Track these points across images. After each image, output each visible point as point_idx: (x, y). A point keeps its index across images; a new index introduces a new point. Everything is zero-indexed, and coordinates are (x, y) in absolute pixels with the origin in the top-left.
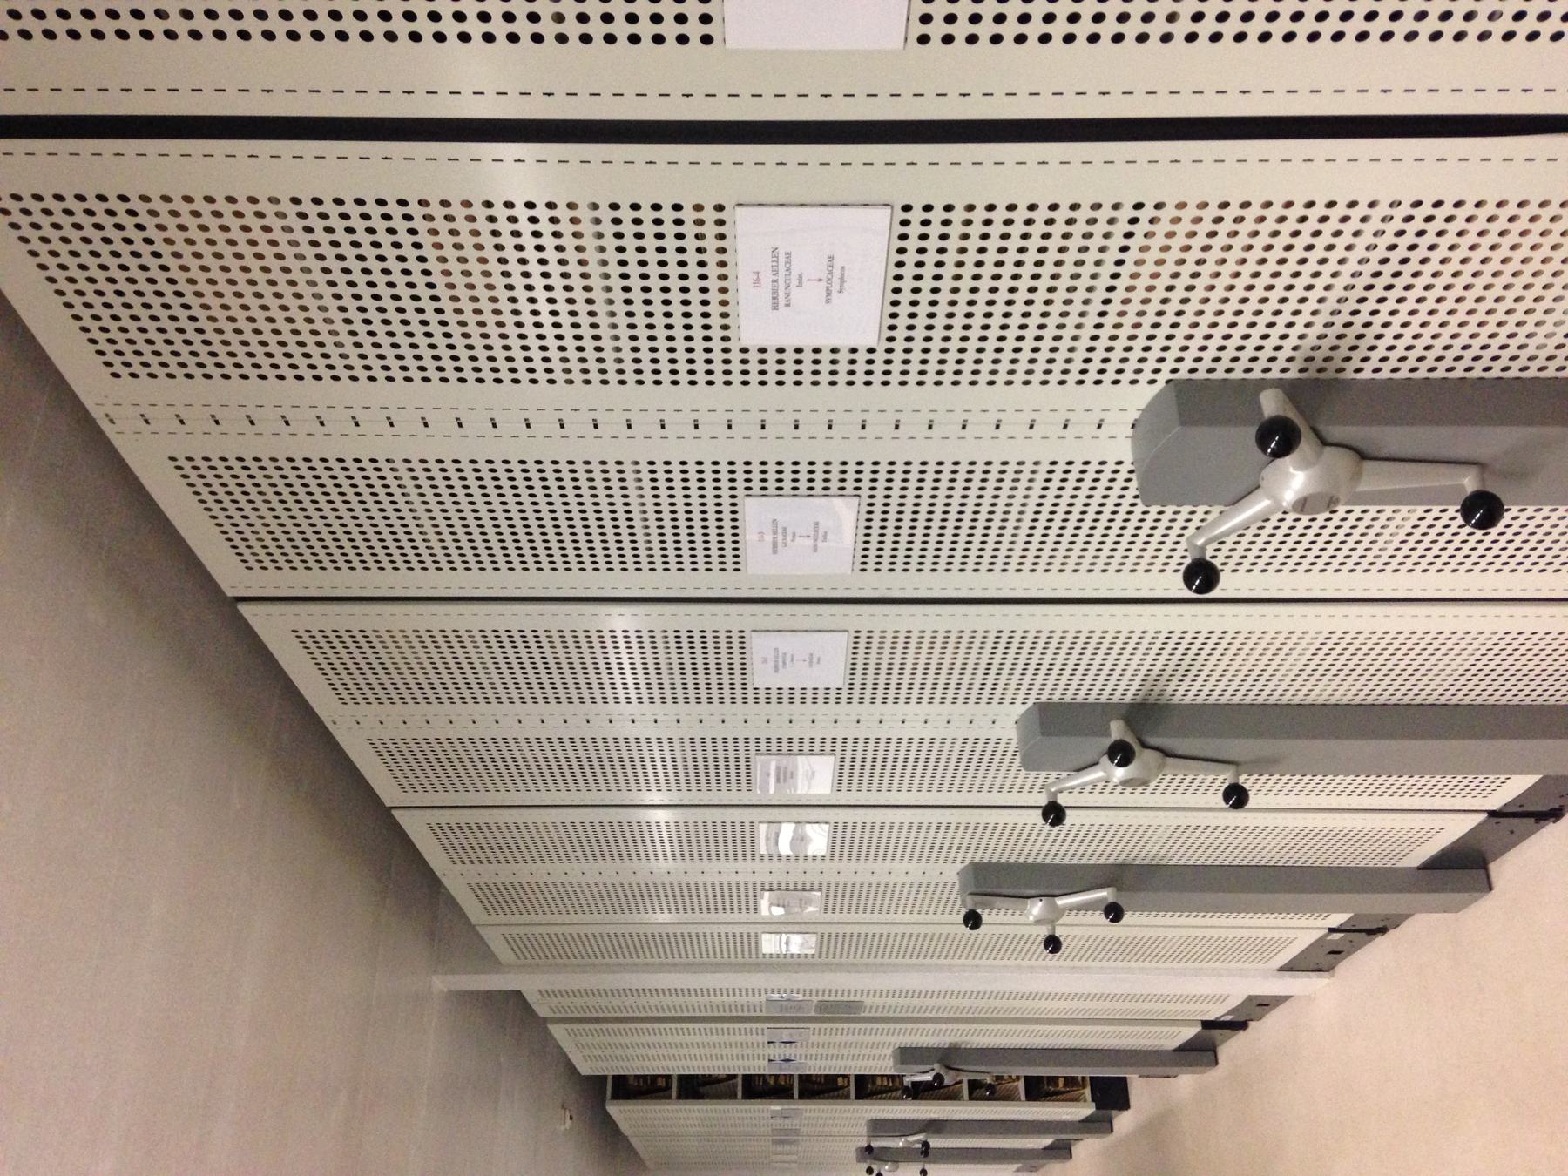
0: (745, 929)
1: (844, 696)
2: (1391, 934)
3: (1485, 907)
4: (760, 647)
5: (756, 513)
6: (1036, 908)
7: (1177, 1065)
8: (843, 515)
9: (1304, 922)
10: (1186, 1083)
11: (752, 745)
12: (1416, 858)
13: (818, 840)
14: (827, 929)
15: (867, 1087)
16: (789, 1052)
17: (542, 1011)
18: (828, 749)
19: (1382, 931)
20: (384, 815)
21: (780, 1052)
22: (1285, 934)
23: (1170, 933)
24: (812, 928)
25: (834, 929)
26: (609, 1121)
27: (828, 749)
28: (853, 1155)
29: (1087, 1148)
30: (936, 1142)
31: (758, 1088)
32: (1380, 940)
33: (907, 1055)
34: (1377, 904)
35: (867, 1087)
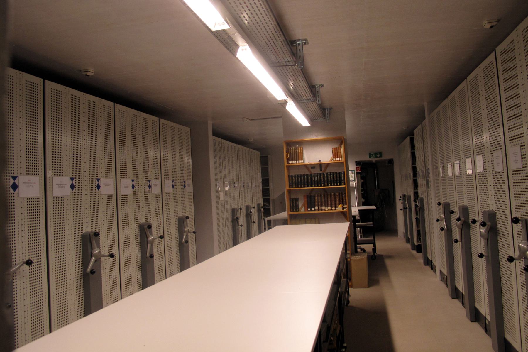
0: (472, 153)
2: (486, 335)
3: (449, 298)
5: (518, 148)
6: (442, 216)
7: (470, 309)
8: (519, 166)
9: (487, 310)
10: (421, 261)
11: (523, 144)
12: (477, 306)
13: (469, 172)
14: (453, 178)
15: (416, 194)
16: (421, 175)
17: (423, 123)
18: (524, 166)
20: (465, 78)
21: (421, 173)
22: (483, 304)
23: (481, 273)
25: (474, 178)
26: (405, 138)
27: (524, 166)
29: (409, 246)
30: (407, 210)
31: (414, 169)
32: (482, 331)
33: (422, 200)
34: (493, 329)
35: (416, 194)
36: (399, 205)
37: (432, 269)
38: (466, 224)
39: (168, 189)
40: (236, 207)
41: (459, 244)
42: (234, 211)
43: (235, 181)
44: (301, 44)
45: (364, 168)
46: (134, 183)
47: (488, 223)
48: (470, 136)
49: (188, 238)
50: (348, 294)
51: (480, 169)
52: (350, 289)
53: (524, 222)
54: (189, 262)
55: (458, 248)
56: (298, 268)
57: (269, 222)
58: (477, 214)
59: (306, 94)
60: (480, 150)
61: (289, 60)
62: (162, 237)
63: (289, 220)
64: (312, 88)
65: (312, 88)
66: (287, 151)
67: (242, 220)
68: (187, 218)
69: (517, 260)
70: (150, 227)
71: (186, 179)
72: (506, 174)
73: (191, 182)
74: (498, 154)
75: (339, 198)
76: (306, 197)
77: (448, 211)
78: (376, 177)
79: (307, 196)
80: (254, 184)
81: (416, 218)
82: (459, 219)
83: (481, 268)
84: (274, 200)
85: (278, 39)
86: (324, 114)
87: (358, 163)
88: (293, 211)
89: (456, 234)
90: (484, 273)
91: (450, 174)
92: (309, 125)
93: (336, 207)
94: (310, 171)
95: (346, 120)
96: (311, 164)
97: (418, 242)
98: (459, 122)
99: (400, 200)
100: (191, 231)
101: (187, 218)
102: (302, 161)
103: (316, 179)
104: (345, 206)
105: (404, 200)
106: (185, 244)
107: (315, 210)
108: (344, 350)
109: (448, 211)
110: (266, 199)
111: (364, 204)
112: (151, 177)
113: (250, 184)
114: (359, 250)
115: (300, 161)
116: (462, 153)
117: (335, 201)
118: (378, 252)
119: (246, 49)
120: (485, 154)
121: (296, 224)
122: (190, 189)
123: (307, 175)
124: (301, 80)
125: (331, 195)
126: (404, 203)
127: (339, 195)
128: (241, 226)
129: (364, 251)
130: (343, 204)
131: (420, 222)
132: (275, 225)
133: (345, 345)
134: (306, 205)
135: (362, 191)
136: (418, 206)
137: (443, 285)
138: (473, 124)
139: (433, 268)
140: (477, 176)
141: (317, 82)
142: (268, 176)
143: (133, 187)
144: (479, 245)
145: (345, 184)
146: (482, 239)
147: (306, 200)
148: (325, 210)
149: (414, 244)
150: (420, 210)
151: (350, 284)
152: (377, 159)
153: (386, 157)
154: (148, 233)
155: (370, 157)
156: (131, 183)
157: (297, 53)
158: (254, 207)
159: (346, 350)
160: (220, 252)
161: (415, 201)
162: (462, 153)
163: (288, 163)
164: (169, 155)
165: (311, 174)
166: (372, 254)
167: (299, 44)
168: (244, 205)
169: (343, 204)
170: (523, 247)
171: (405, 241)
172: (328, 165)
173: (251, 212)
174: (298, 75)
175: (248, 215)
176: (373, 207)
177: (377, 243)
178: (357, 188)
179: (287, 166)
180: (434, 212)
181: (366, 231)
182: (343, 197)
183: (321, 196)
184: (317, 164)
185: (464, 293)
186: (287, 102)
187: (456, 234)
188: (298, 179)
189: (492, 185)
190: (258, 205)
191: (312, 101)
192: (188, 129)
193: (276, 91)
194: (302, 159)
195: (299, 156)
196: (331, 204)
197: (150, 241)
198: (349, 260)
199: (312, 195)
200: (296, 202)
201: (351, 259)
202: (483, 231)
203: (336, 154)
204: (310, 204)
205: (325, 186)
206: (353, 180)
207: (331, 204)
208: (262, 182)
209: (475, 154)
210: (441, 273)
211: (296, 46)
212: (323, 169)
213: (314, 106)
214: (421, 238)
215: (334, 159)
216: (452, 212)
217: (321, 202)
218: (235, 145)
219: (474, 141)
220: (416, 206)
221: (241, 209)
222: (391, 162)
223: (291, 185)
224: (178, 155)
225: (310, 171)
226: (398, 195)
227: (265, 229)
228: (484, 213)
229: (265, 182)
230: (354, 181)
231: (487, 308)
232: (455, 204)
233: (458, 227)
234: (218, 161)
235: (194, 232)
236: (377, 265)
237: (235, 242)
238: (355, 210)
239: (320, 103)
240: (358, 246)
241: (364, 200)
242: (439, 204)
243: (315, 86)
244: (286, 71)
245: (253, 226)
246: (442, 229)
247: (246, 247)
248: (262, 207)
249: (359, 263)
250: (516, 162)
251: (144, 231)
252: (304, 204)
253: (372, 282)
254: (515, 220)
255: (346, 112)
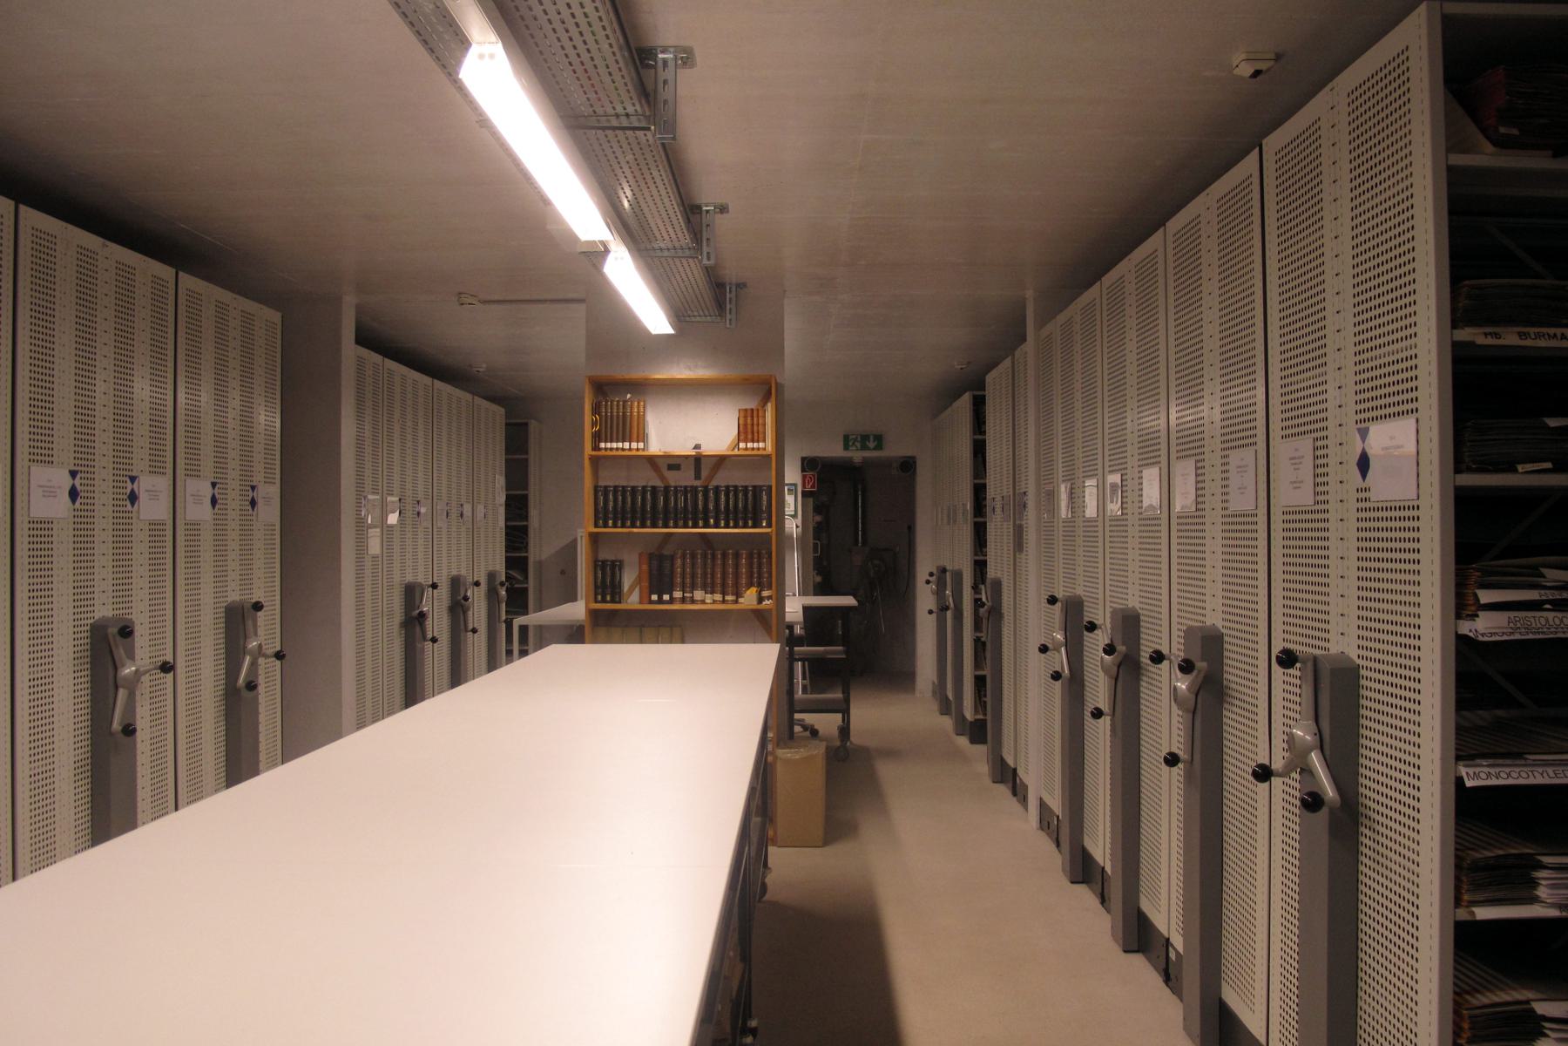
1: (1364, 505)
4: (1247, 456)
5: (1305, 445)
6: (1059, 637)
8: (1305, 497)
9: (1174, 921)
10: (983, 768)
12: (1145, 906)
15: (980, 566)
16: (998, 511)
17: (1018, 353)
18: (1320, 498)
19: (1167, 979)
20: (1161, 223)
22: (1164, 902)
23: (1165, 810)
24: (1165, 509)
27: (1320, 498)
28: (941, 563)
29: (947, 723)
30: (949, 614)
31: (979, 492)
33: (997, 586)
35: (980, 566)
36: (925, 599)
37: (1015, 794)
38: (1129, 668)
39: (198, 510)
40: (421, 579)
41: (1105, 721)
42: (411, 593)
43: (421, 497)
44: (671, 64)
45: (831, 483)
46: (77, 482)
47: (1201, 665)
48: (1163, 401)
49: (256, 676)
50: (766, 865)
51: (1183, 500)
52: (771, 849)
53: (1310, 665)
54: (256, 751)
55: (1100, 735)
56: (626, 784)
57: (524, 630)
58: (1165, 636)
59: (669, 228)
60: (1190, 444)
61: (630, 110)
62: (167, 668)
63: (587, 630)
64: (692, 212)
65: (692, 212)
66: (596, 410)
67: (438, 623)
68: (258, 607)
69: (1280, 775)
70: (126, 632)
71: (258, 478)
72: (1262, 519)
73: (274, 490)
74: (1245, 458)
75: (750, 565)
76: (656, 561)
77: (1076, 622)
78: (861, 508)
79: (651, 556)
80: (480, 509)
81: (977, 641)
82: (1110, 650)
83: (1166, 795)
84: (540, 564)
85: (601, 34)
86: (717, 302)
87: (808, 464)
88: (603, 601)
89: (1099, 691)
90: (1175, 810)
91: (1091, 511)
92: (670, 331)
93: (738, 595)
94: (663, 478)
95: (786, 325)
96: (667, 457)
97: (976, 712)
98: (1131, 357)
99: (928, 582)
100: (271, 651)
101: (258, 607)
102: (641, 445)
103: (681, 504)
104: (765, 593)
105: (941, 584)
106: (246, 694)
107: (672, 600)
108: (749, 1040)
109: (1076, 622)
110: (517, 561)
111: (821, 590)
112: (140, 463)
113: (467, 509)
114: (797, 729)
115: (634, 445)
116: (1132, 450)
117: (737, 575)
118: (855, 739)
119: (492, 56)
120: (1206, 457)
121: (609, 640)
122: (270, 512)
123: (654, 488)
124: (658, 180)
125: (724, 556)
126: (939, 593)
127: (750, 556)
128: (434, 640)
129: (814, 733)
130: (761, 586)
131: (987, 650)
132: (540, 645)
133: (753, 1023)
134: (646, 584)
135: (815, 550)
136: (983, 605)
137: (1047, 844)
138: (1172, 364)
139: (1019, 792)
140: (1174, 521)
141: (708, 193)
142: (526, 487)
143: (74, 494)
144: (1165, 727)
145: (769, 525)
146: (1174, 707)
147: (645, 567)
148: (703, 602)
149: (964, 717)
150: (989, 616)
151: (771, 833)
152: (867, 454)
153: (895, 449)
154: (120, 653)
155: (846, 447)
156: (67, 482)
157: (655, 91)
158: (477, 584)
159: (754, 1037)
160: (361, 725)
161: (975, 588)
162: (1132, 450)
163: (596, 448)
164: (206, 398)
165: (667, 488)
166: (838, 743)
167: (665, 62)
168: (445, 573)
169: (761, 586)
170: (1303, 739)
171: (935, 706)
172: (720, 461)
173: (466, 598)
174: (650, 161)
175: (458, 607)
176: (849, 601)
177: (855, 712)
178: (802, 539)
179: (591, 458)
180: (1031, 626)
181: (821, 672)
182: (759, 564)
183: (693, 557)
184: (687, 457)
185: (1108, 869)
186: (607, 251)
187: (1099, 691)
188: (644, 499)
189: (1219, 550)
190: (491, 576)
191: (687, 252)
192: (276, 317)
193: (578, 209)
194: (642, 437)
195: (630, 428)
196: (724, 585)
197: (125, 678)
198: (770, 759)
199: (666, 552)
200: (613, 574)
201: (776, 758)
202: (1182, 686)
203: (748, 428)
204: (659, 579)
205: (706, 525)
206: (793, 517)
207: (724, 585)
208: (507, 505)
209: (1173, 456)
210: (1043, 805)
211: (654, 67)
212: (704, 473)
213: (691, 273)
214: (988, 699)
215: (742, 445)
216: (1092, 627)
217: (693, 576)
218: (427, 380)
219: (1173, 416)
220: (978, 603)
221: (434, 586)
222: (908, 465)
223: (601, 516)
224: (235, 401)
225: (663, 478)
226: (924, 567)
227: (509, 652)
228: (1189, 632)
229: (517, 506)
230: (795, 516)
231: (1174, 914)
232: (1101, 602)
233: (1106, 671)
234: (367, 427)
235: (279, 656)
236: (850, 779)
237: (412, 694)
238: (794, 608)
239: (712, 262)
240: (797, 716)
241: (819, 579)
242: (1052, 600)
243: (699, 207)
244: (615, 146)
245: (470, 642)
246: (1056, 676)
247: (442, 712)
248: (502, 584)
249: (803, 765)
250: (1297, 484)
251: (107, 644)
252: (639, 580)
253: (836, 829)
254: (1288, 659)
255: (786, 301)
